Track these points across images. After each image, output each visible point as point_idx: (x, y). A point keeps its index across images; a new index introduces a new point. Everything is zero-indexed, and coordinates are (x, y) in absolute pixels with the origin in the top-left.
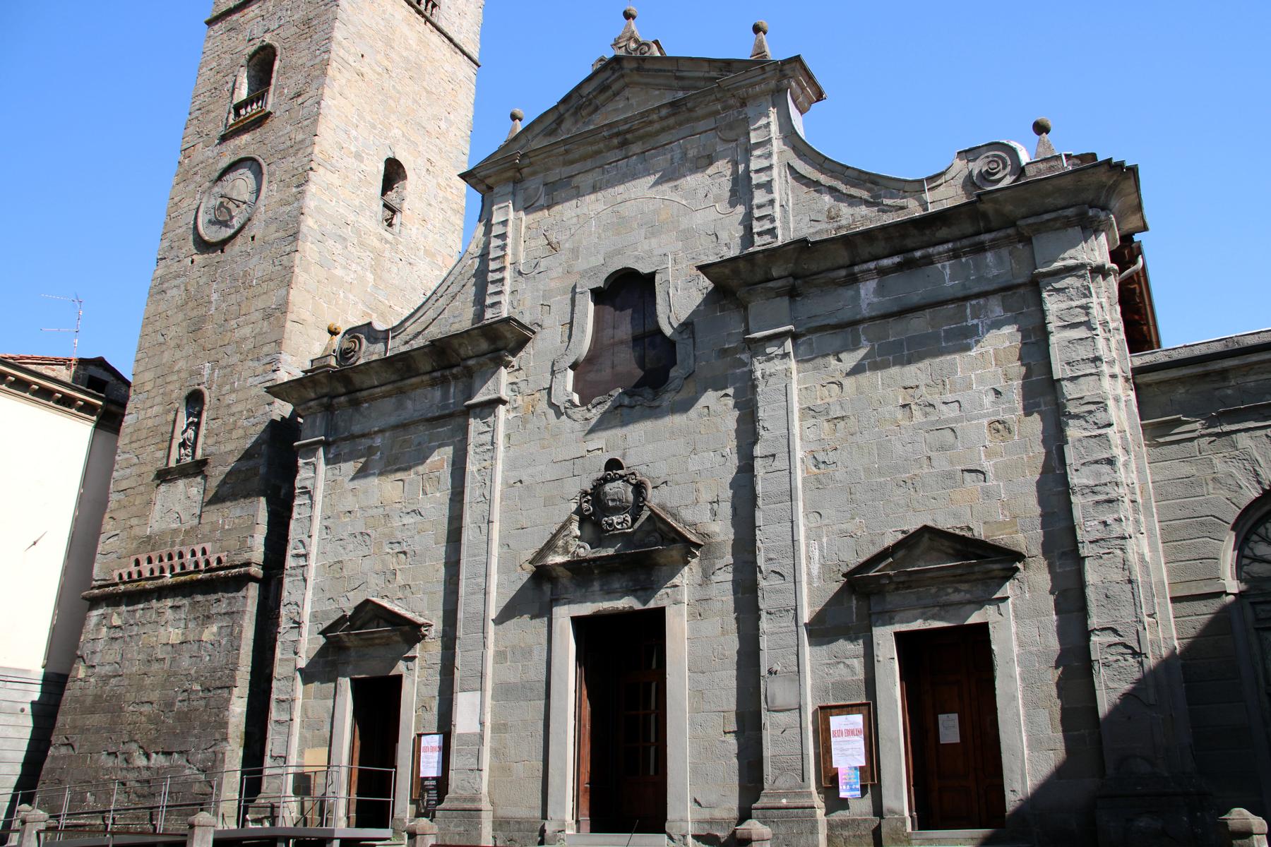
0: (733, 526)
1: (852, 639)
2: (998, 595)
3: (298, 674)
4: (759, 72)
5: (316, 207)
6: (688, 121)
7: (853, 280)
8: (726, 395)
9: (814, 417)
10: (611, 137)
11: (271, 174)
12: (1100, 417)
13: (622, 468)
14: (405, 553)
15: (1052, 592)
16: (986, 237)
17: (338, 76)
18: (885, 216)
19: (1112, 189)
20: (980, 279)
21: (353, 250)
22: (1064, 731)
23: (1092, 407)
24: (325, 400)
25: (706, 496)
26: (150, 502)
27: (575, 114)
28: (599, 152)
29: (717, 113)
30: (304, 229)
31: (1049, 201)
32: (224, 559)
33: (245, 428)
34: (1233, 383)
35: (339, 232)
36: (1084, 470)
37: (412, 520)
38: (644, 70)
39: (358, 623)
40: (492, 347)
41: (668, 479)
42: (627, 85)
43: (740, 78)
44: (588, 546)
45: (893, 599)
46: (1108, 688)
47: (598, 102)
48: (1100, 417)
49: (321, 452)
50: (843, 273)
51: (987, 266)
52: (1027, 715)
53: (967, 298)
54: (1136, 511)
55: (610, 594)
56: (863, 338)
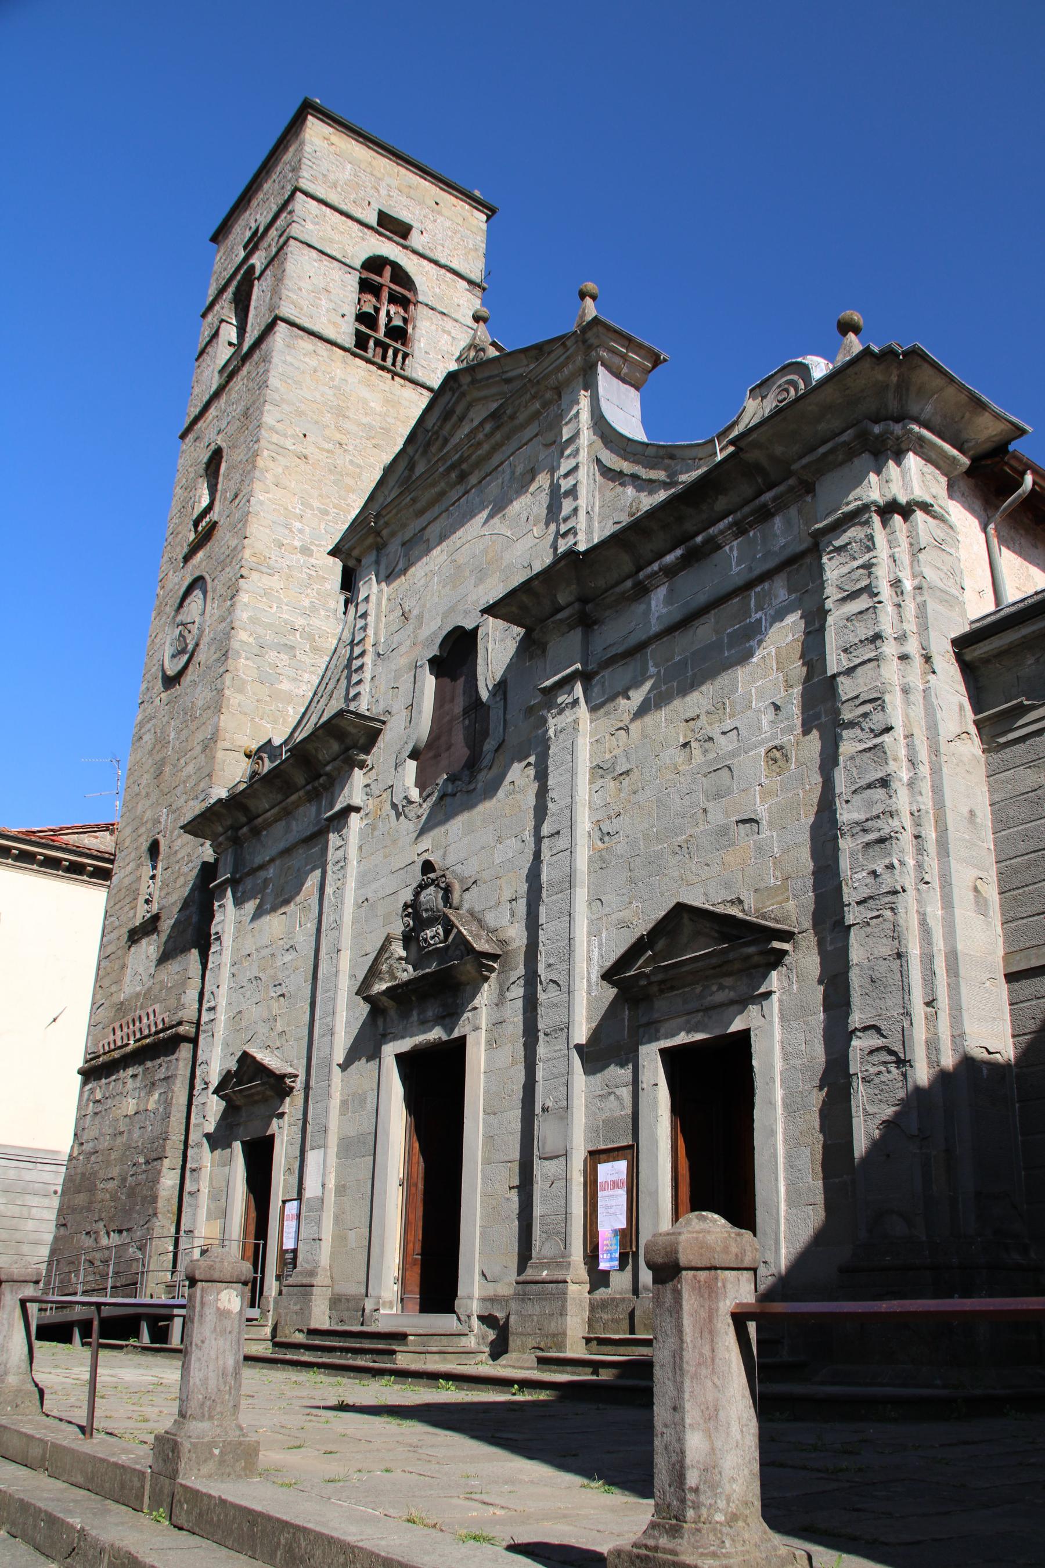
0: (527, 929)
1: (622, 1065)
2: (762, 990)
3: (205, 1140)
4: (561, 351)
5: (250, 618)
7: (642, 591)
8: (529, 764)
9: (602, 777)
11: (214, 591)
12: (877, 720)
13: (434, 871)
14: (283, 995)
15: (820, 982)
16: (767, 496)
17: (271, 465)
18: (656, 496)
19: (903, 387)
21: (304, 658)
22: (824, 1179)
23: (868, 708)
25: (507, 894)
26: (123, 967)
27: (425, 452)
28: (442, 494)
30: (235, 644)
31: (822, 427)
35: (284, 641)
36: (857, 799)
37: (290, 957)
38: (480, 381)
39: (245, 1078)
40: (343, 747)
41: (478, 877)
42: (469, 406)
43: (546, 363)
44: (410, 968)
45: (661, 1004)
46: (866, 1113)
47: (445, 432)
48: (877, 720)
49: (229, 893)
50: (629, 583)
52: (788, 1156)
54: (920, 850)
55: (425, 1025)
56: (651, 663)
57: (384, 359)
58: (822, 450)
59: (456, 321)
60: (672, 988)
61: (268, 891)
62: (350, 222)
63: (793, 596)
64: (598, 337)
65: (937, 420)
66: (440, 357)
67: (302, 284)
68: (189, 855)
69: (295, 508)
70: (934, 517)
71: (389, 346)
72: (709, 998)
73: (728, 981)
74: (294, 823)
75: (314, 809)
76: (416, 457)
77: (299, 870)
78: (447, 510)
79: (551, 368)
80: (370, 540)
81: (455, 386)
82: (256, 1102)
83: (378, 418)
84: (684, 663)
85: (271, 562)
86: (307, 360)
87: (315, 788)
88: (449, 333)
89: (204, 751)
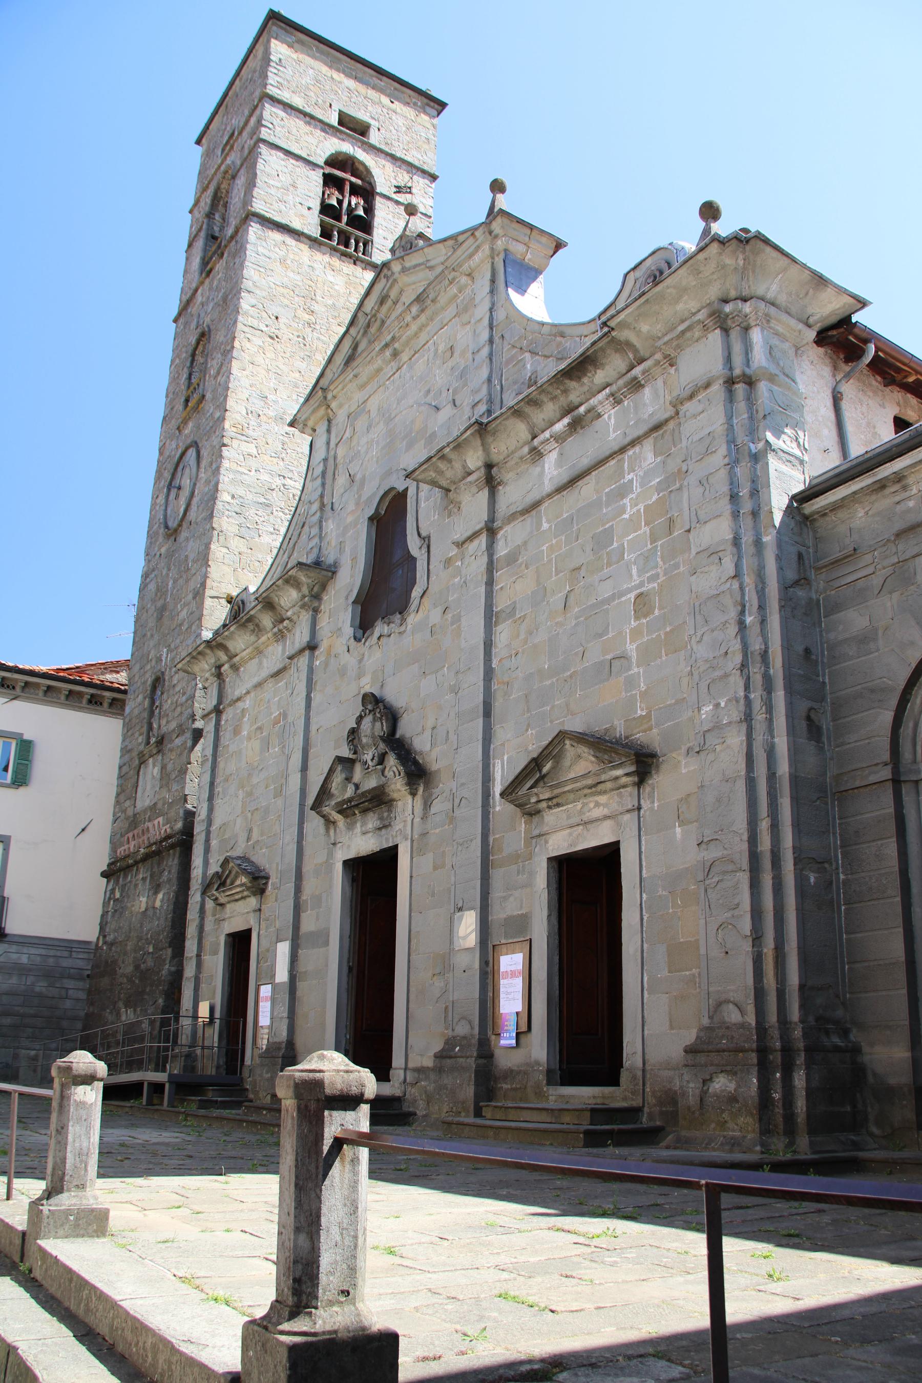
4: (471, 240)
6: (436, 313)
7: (537, 454)
16: (637, 371)
17: (248, 345)
28: (379, 370)
29: (456, 296)
32: (168, 830)
33: (182, 705)
34: (915, 491)
40: (300, 595)
47: (381, 315)
51: (645, 405)
53: (622, 450)
56: (544, 520)
58: (681, 328)
60: (558, 805)
61: (245, 719)
65: (782, 299)
68: (183, 688)
72: (588, 814)
73: (602, 799)
74: (265, 660)
75: (280, 648)
76: (358, 338)
77: (269, 701)
79: (463, 257)
80: (322, 411)
81: (389, 273)
87: (280, 630)
89: (194, 598)
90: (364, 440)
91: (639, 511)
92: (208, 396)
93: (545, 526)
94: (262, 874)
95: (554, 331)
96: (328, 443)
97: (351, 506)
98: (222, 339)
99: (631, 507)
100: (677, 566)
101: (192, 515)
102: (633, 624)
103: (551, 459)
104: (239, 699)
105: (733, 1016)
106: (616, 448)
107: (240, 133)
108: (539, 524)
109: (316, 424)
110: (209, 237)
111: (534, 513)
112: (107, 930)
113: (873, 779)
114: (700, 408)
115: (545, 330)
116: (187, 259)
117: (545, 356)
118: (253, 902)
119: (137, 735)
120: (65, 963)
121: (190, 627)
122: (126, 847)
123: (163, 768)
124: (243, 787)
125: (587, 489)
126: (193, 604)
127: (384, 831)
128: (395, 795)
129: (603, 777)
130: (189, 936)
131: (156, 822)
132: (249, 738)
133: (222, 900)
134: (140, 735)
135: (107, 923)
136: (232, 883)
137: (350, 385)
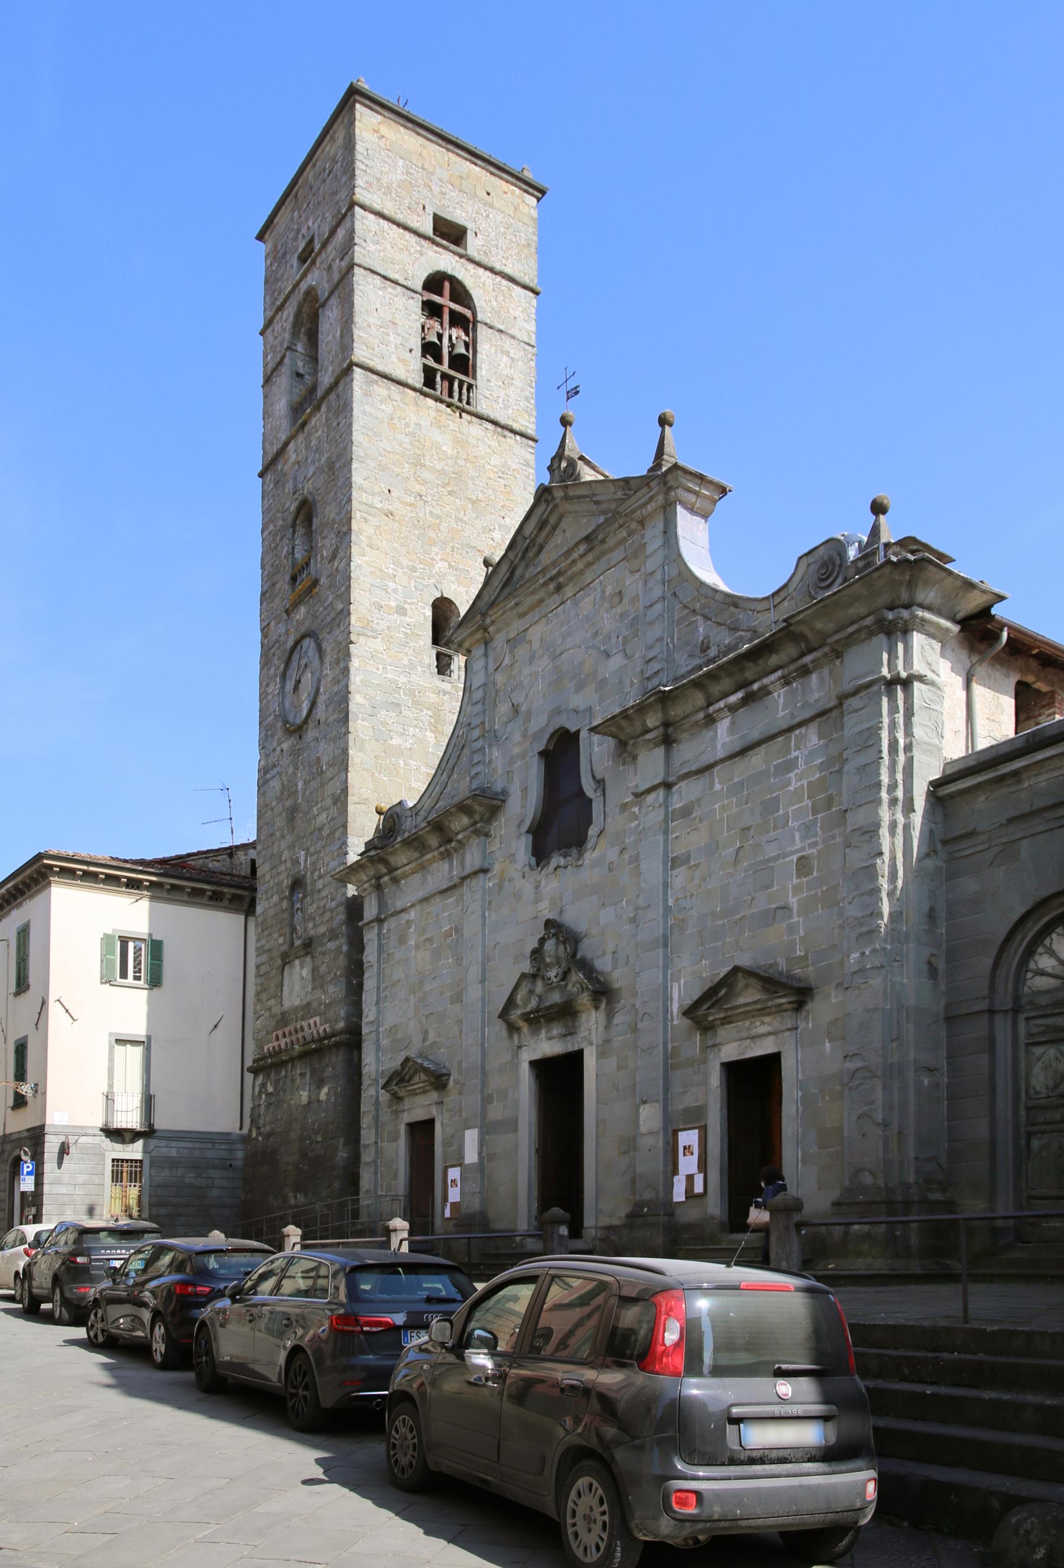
6: (603, 553)
7: (711, 721)
10: (545, 584)
16: (807, 659)
17: (364, 526)
20: (806, 704)
24: (373, 881)
32: (328, 1030)
33: (331, 910)
47: (540, 540)
50: (701, 715)
53: (791, 729)
56: (716, 781)
57: (451, 395)
58: (850, 630)
59: (513, 337)
60: (730, 1023)
61: (412, 930)
62: (408, 235)
63: (822, 742)
64: (677, 480)
66: (500, 383)
67: (371, 320)
69: (388, 568)
70: (926, 684)
71: (454, 378)
73: (767, 1019)
74: (429, 877)
75: (446, 866)
77: (437, 915)
78: (546, 616)
80: (479, 635)
81: (550, 498)
82: (417, 1094)
83: (451, 462)
84: (741, 783)
85: (374, 625)
86: (383, 407)
87: (447, 850)
88: (508, 354)
89: (335, 804)
90: (526, 671)
91: (803, 785)
92: (323, 580)
93: (718, 787)
94: (444, 1071)
95: (728, 600)
96: (486, 668)
97: (517, 737)
98: (332, 516)
99: (796, 781)
100: (833, 837)
101: (320, 712)
102: (795, 881)
103: (723, 726)
104: (403, 911)
105: (867, 1179)
106: (785, 727)
107: (324, 246)
108: (712, 785)
109: (472, 645)
110: (294, 376)
111: (707, 773)
112: (261, 1122)
113: (975, 1009)
114: (861, 705)
115: (718, 597)
116: (265, 396)
117: (718, 623)
118: (434, 1096)
119: (276, 935)
120: (210, 1154)
121: (332, 832)
122: (276, 1044)
123: (315, 970)
124: (414, 993)
125: (757, 760)
126: (334, 811)
127: (569, 1038)
128: (580, 1008)
129: (770, 1004)
130: (364, 1126)
131: (312, 1021)
132: (417, 947)
133: (401, 1094)
134: (281, 936)
135: (259, 1116)
136: (409, 1081)
137: (509, 613)
